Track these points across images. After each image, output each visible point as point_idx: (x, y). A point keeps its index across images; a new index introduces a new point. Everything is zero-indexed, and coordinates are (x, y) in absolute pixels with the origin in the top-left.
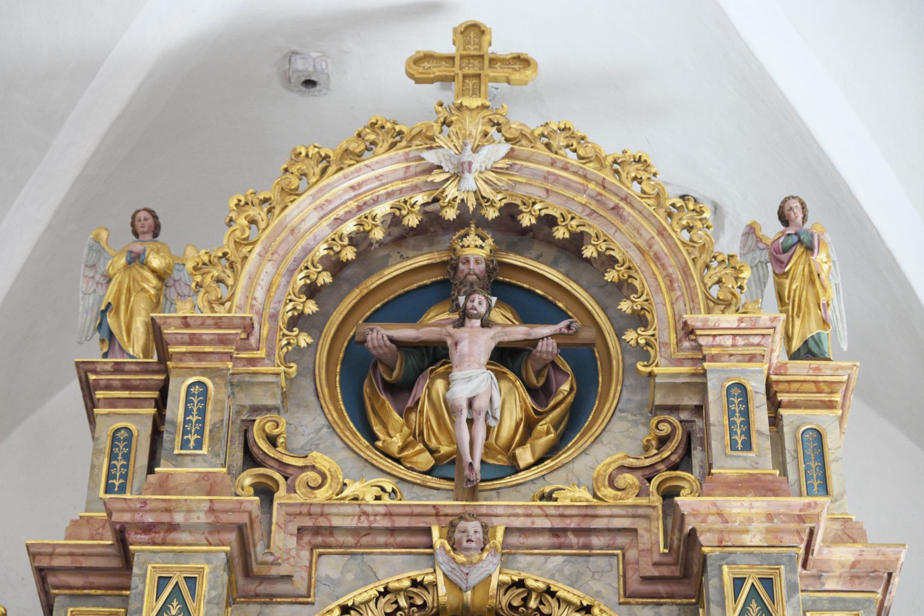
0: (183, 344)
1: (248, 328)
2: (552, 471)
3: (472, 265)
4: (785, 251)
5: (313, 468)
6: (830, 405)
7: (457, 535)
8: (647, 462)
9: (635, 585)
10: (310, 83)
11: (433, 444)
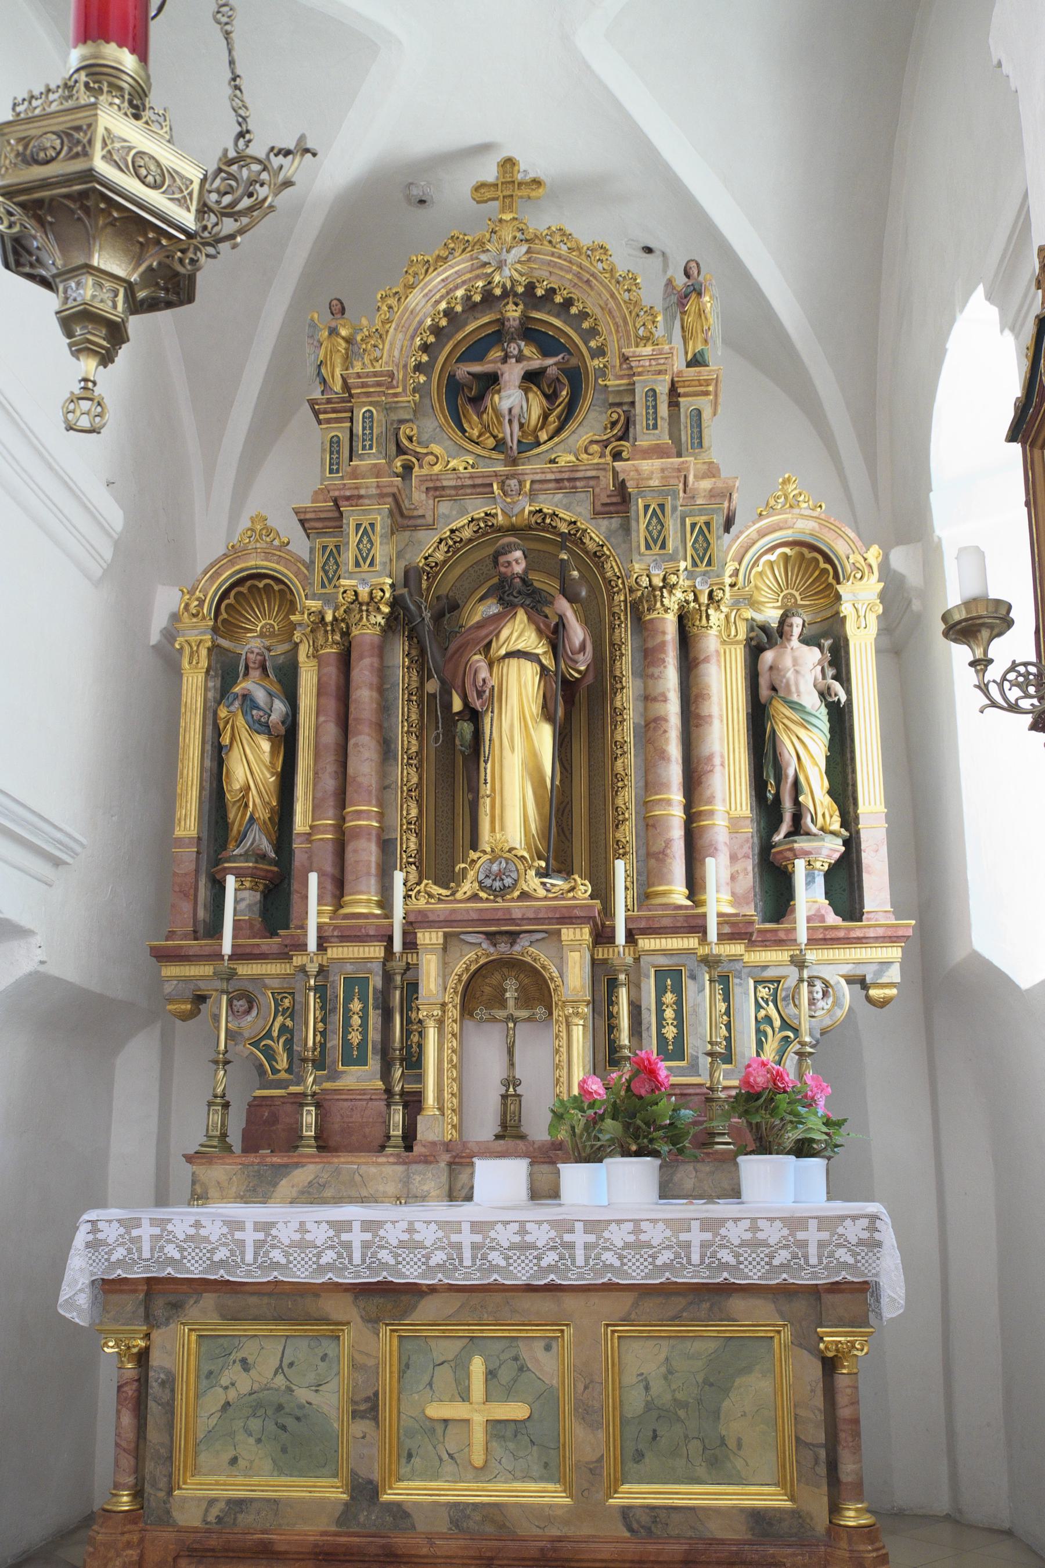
0: (358, 387)
1: (391, 375)
2: (557, 444)
3: (511, 322)
4: (686, 297)
5: (432, 453)
6: (706, 393)
7: (506, 488)
8: (605, 437)
9: (599, 508)
10: (422, 202)
11: (495, 432)
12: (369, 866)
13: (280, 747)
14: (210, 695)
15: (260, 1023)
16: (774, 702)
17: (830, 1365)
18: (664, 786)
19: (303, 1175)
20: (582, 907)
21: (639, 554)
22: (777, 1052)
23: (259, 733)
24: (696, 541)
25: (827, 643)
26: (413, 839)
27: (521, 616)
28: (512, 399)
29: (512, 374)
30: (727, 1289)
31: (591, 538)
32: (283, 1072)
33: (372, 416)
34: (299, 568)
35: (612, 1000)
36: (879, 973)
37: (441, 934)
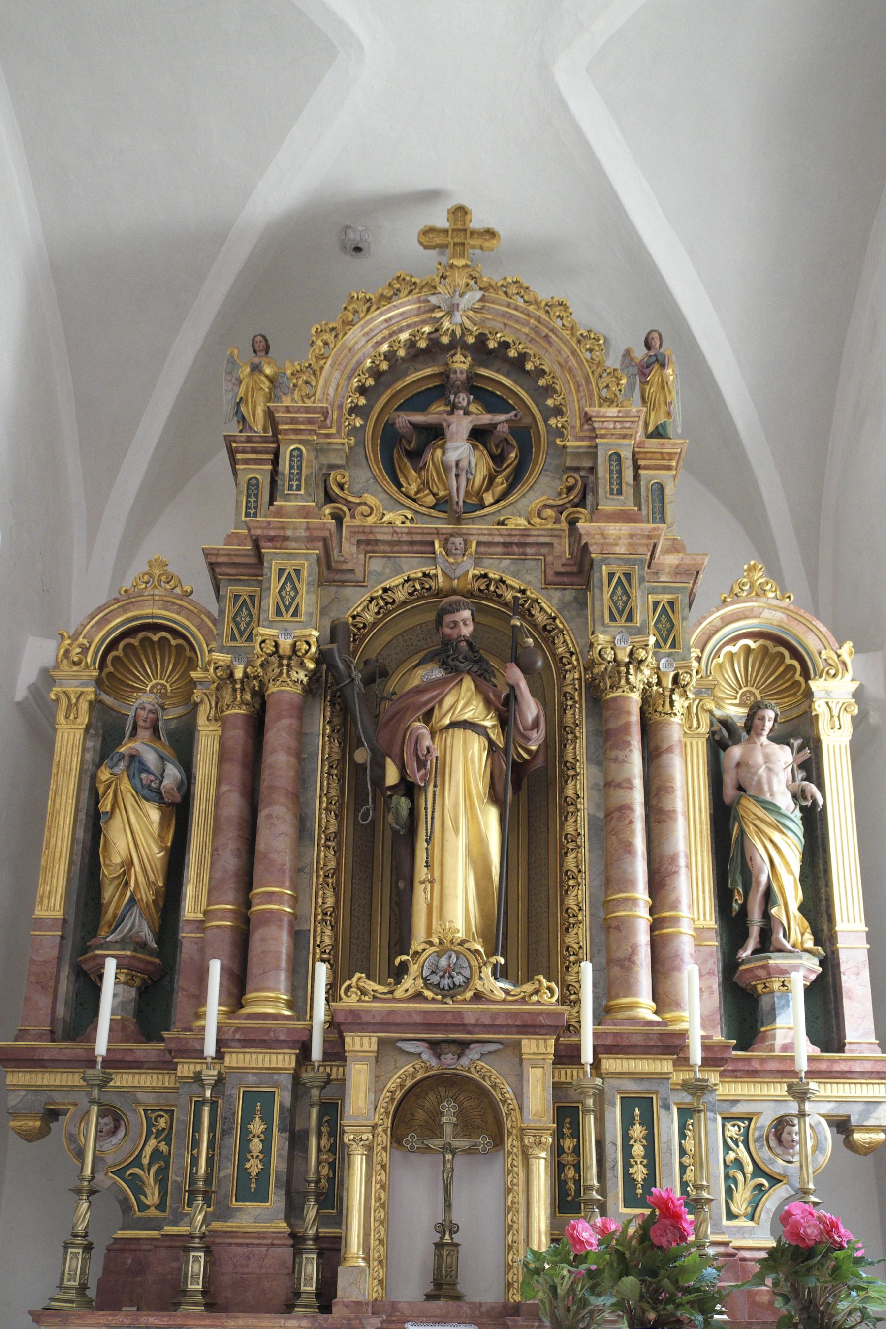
0: (287, 423)
1: (325, 413)
2: (504, 507)
3: (458, 375)
4: (648, 367)
5: (365, 504)
6: (669, 468)
8: (560, 502)
9: (551, 577)
10: (358, 249)
12: (278, 958)
13: (170, 820)
14: (89, 756)
15: (128, 1146)
16: (744, 802)
18: (628, 883)
20: (548, 1014)
21: (603, 624)
22: (750, 1203)
23: (147, 800)
24: (658, 620)
26: (328, 932)
27: (468, 683)
28: (459, 451)
31: (542, 609)
32: (152, 1209)
33: (301, 455)
34: (203, 620)
36: (866, 1114)
37: (374, 1040)
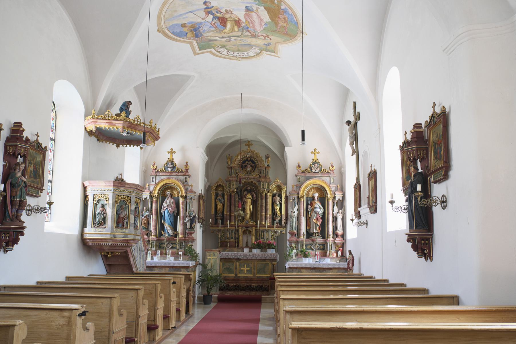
17: (273, 265)
19: (228, 249)
25: (280, 196)
29: (249, 166)
30: (266, 259)
35: (257, 233)
36: (283, 231)
